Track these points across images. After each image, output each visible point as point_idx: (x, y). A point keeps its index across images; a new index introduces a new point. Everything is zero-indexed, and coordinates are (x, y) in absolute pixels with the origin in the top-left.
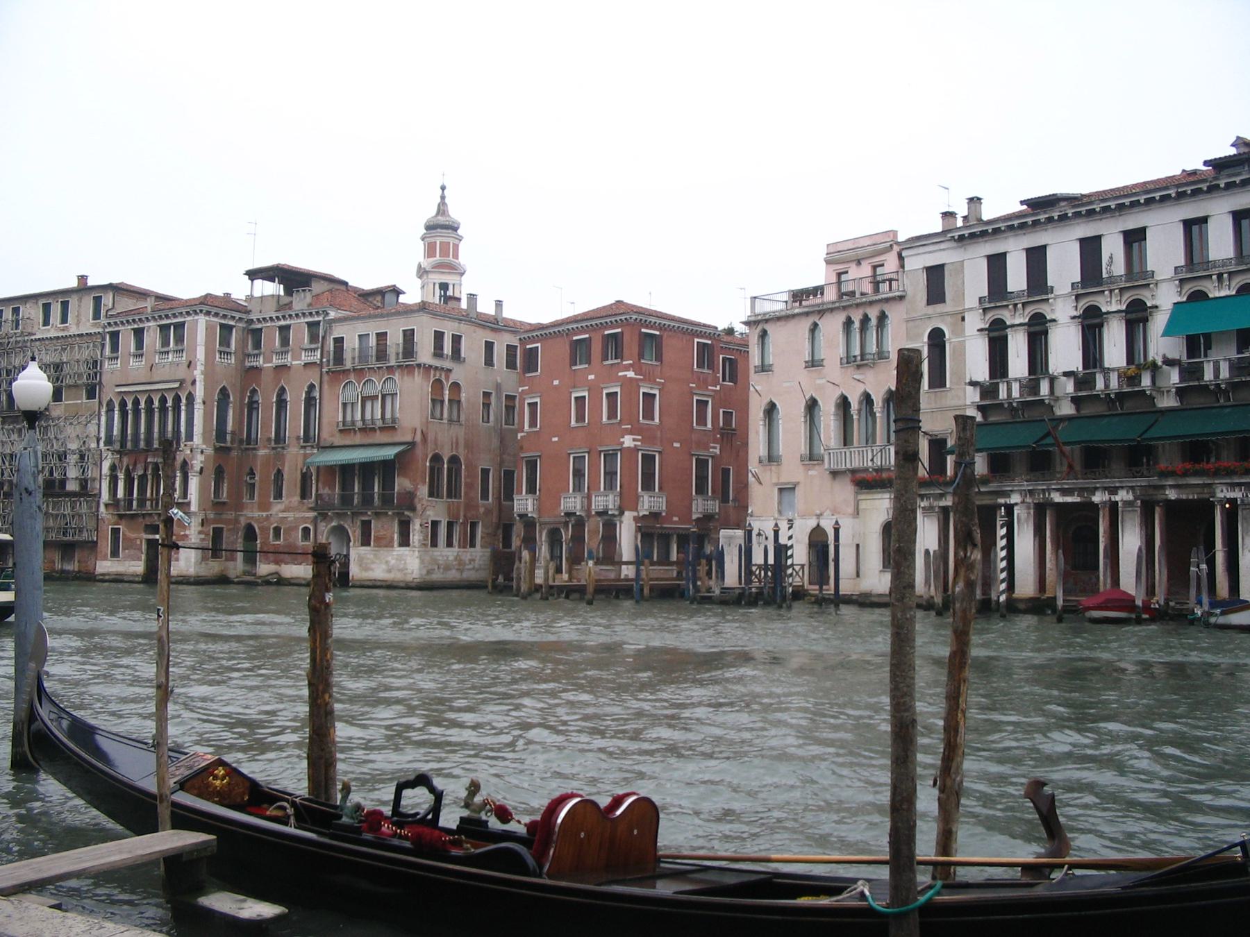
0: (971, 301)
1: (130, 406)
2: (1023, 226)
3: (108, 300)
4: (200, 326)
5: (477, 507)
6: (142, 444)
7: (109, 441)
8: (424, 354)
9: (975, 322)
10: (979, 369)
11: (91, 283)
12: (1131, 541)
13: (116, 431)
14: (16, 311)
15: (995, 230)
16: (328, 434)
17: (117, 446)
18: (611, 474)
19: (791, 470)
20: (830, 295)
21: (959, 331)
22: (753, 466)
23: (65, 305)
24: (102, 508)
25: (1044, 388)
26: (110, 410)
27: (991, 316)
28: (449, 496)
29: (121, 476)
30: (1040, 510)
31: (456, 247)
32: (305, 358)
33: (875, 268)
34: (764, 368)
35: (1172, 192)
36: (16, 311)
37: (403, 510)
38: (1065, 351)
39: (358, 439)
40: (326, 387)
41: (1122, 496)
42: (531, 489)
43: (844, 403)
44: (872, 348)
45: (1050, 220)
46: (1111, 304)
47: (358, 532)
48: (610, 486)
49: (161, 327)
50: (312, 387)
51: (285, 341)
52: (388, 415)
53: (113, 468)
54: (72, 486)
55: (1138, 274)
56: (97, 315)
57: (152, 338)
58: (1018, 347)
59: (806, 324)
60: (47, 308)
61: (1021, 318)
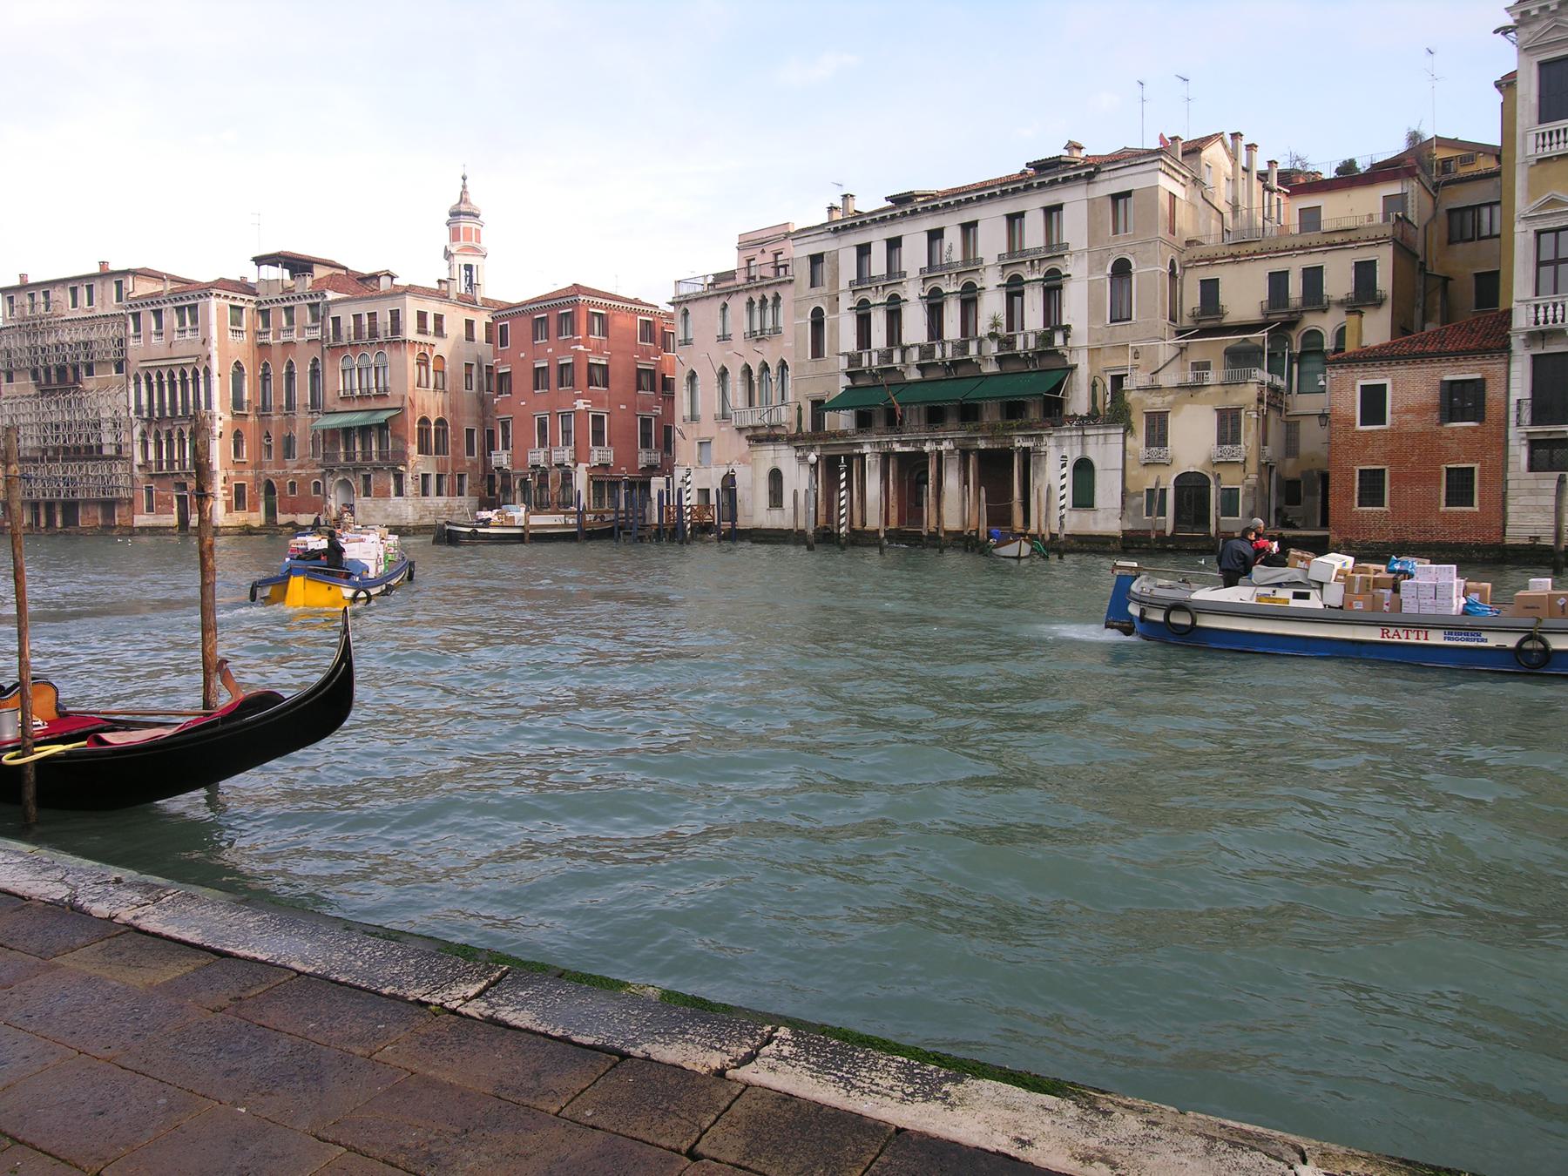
0: (843, 284)
1: (154, 379)
3: (129, 283)
4: (215, 308)
5: (463, 462)
6: (168, 413)
7: (139, 410)
8: (410, 331)
9: (847, 301)
10: (849, 342)
11: (30, 281)
12: (952, 481)
13: (144, 401)
14: (46, 294)
16: (330, 401)
17: (145, 415)
18: (567, 432)
19: (708, 428)
20: (741, 279)
21: (834, 309)
22: (679, 424)
23: (90, 288)
24: (136, 470)
25: (973, 349)
26: (138, 383)
27: (1009, 272)
29: (151, 441)
30: (886, 457)
32: (308, 335)
33: (776, 255)
34: (687, 342)
35: (997, 190)
36: (46, 294)
37: (394, 465)
38: (915, 327)
39: (356, 405)
41: (946, 446)
42: (506, 447)
43: (748, 371)
44: (769, 325)
45: (904, 214)
46: (950, 286)
47: (361, 485)
48: (567, 443)
50: (315, 360)
51: (291, 321)
52: (381, 384)
53: (144, 434)
54: (107, 451)
55: (971, 261)
56: (119, 299)
57: (171, 319)
59: (718, 303)
60: (74, 290)
61: (882, 299)
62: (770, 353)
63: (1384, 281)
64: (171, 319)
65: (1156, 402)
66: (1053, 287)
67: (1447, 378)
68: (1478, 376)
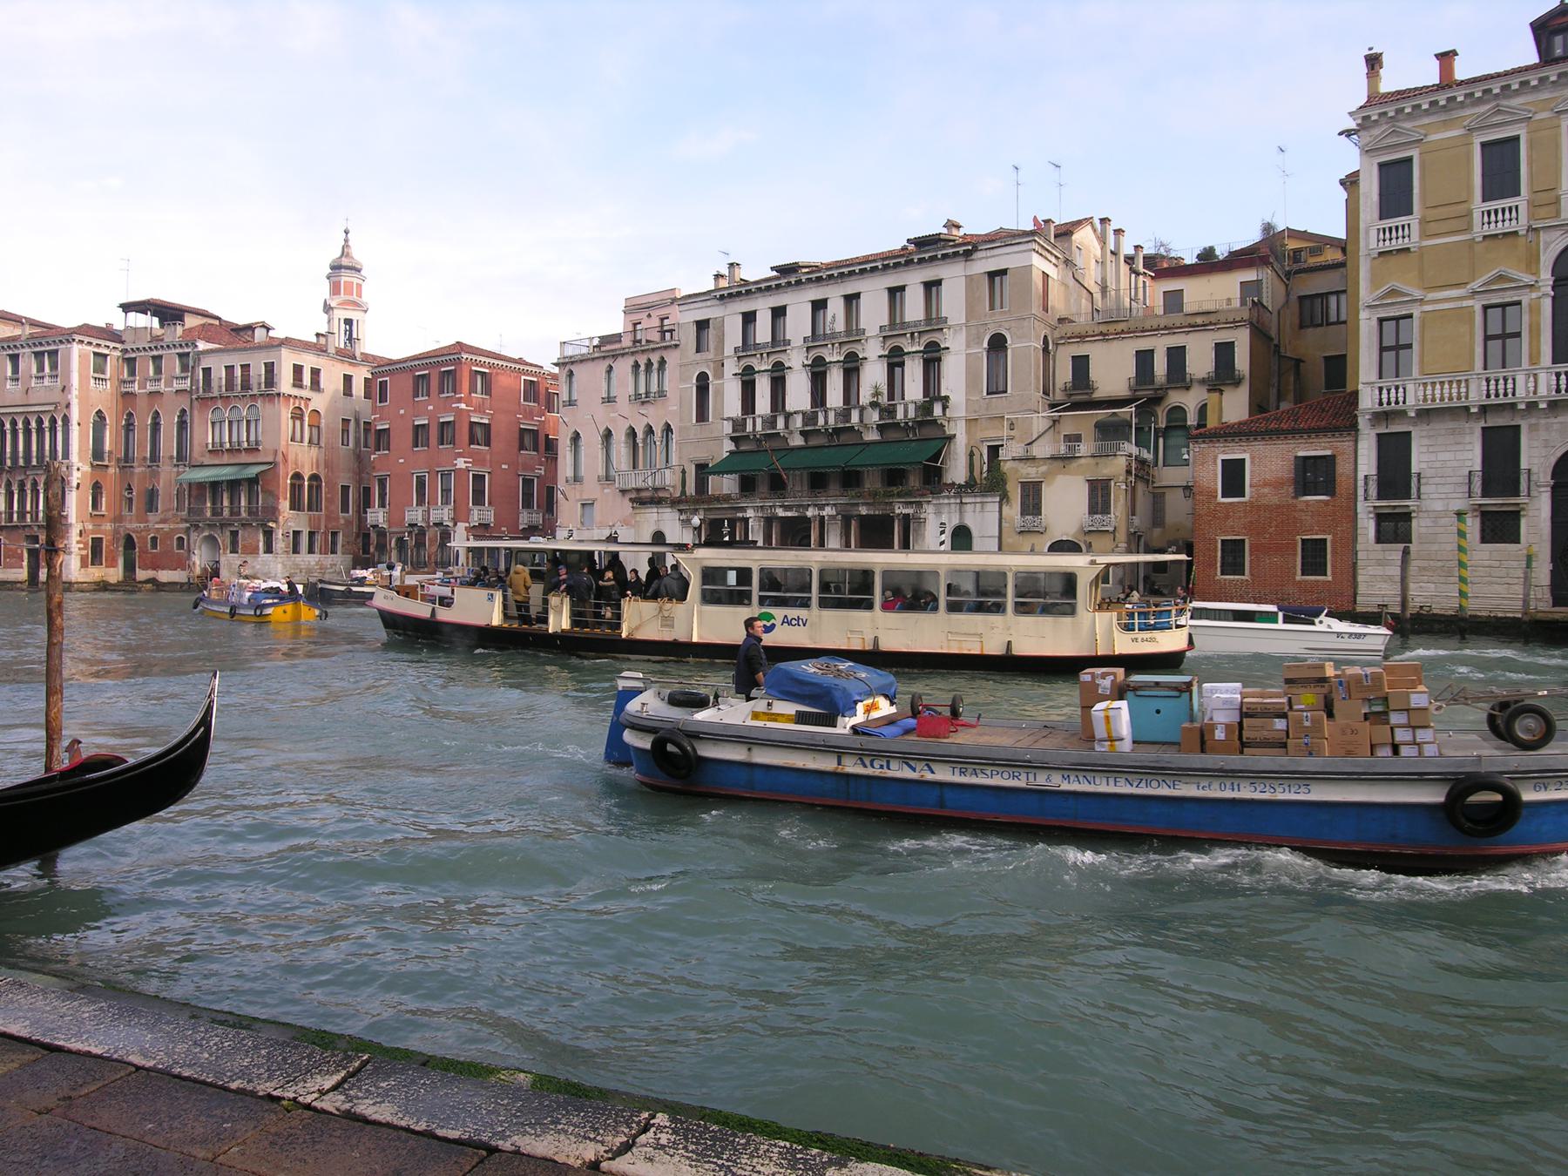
0: (729, 350)
2: (769, 288)
4: (77, 355)
5: (337, 519)
6: (21, 462)
8: (285, 384)
9: (732, 367)
10: (733, 407)
15: (746, 290)
16: (197, 453)
18: (446, 491)
19: (591, 489)
20: (627, 342)
22: (561, 485)
25: (855, 417)
27: (890, 343)
28: (310, 509)
31: (359, 286)
32: (177, 385)
35: (879, 264)
37: (264, 521)
38: (798, 394)
39: (226, 459)
40: (196, 413)
41: (828, 511)
42: (382, 505)
43: (632, 433)
44: (654, 388)
45: (789, 284)
46: (833, 356)
47: (228, 541)
48: (446, 502)
49: (36, 354)
50: (183, 411)
51: (158, 370)
52: (252, 438)
57: (28, 364)
58: (763, 388)
59: (604, 365)
62: (655, 416)
63: (1242, 362)
64: (28, 364)
65: (1030, 472)
66: (932, 359)
67: (1301, 454)
68: (1328, 453)
